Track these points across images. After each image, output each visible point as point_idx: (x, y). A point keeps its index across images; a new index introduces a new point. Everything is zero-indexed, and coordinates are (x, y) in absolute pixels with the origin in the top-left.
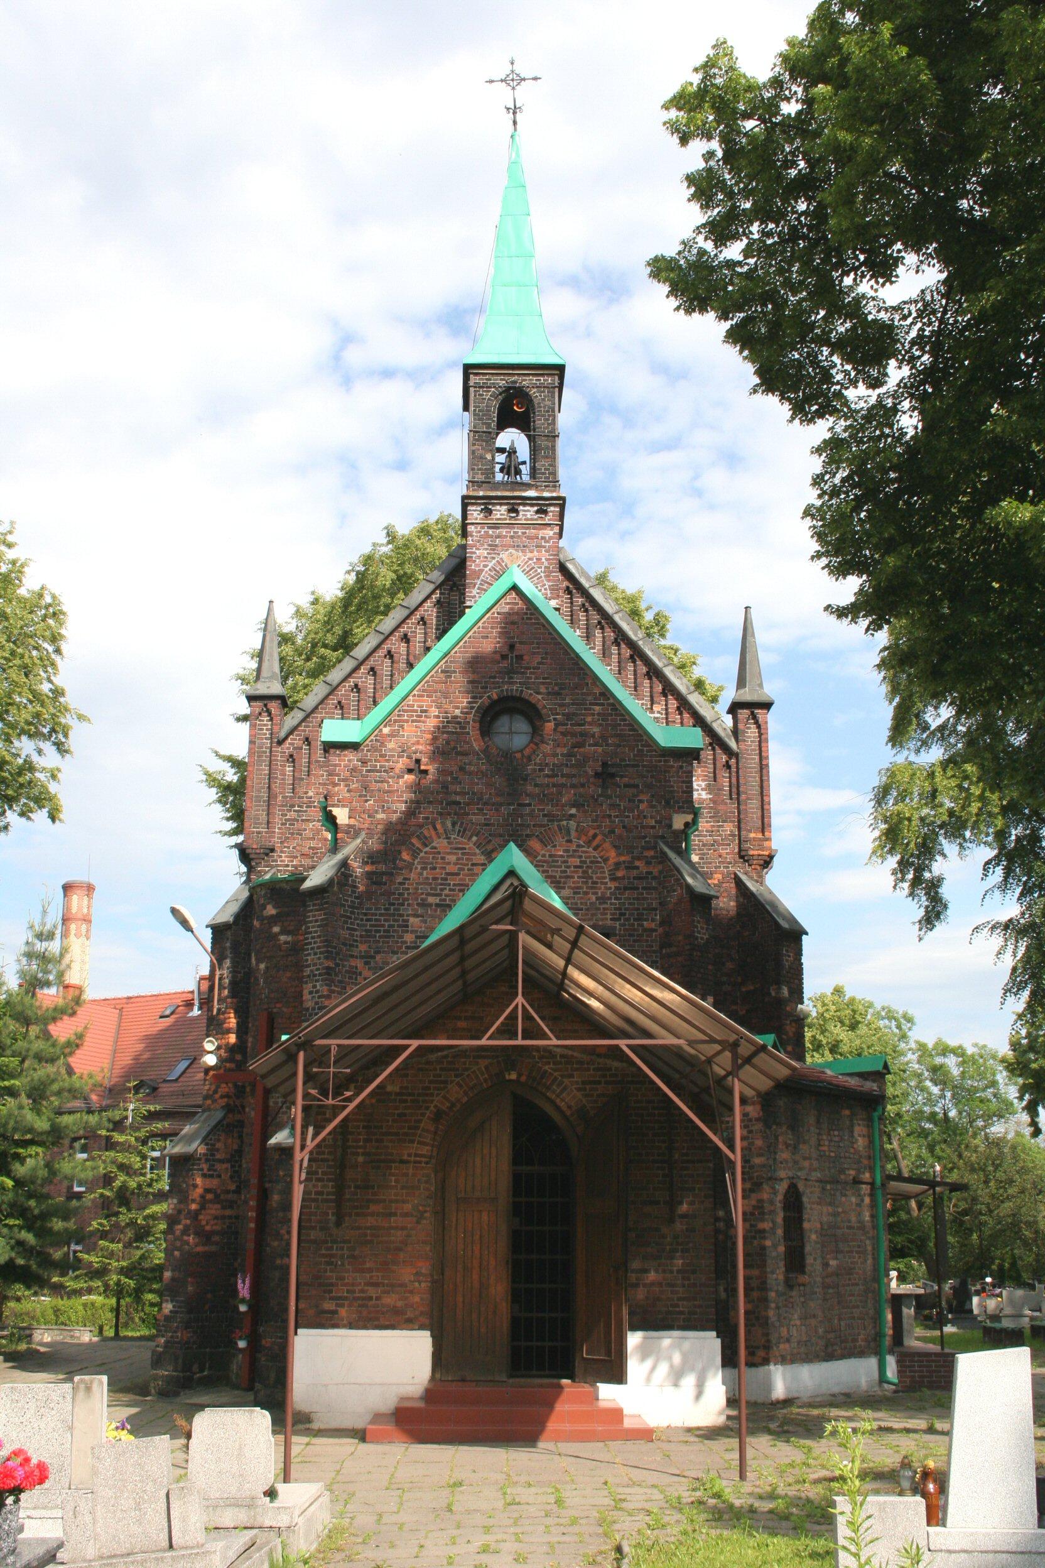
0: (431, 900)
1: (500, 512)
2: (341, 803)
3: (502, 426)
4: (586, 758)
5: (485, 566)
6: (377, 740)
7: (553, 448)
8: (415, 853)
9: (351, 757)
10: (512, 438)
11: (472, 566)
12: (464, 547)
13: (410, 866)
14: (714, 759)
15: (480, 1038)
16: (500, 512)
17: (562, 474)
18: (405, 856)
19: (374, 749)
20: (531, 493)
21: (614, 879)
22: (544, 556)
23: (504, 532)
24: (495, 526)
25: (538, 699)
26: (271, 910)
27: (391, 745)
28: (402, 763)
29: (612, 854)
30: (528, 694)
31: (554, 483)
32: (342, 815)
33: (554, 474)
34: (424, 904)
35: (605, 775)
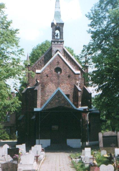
0: (49, 91)
1: (56, 43)
2: (38, 80)
3: (56, 30)
4: (67, 75)
5: (63, 78)
6: (42, 73)
7: (63, 34)
8: (47, 86)
9: (40, 75)
10: (57, 32)
11: (53, 49)
12: (51, 46)
13: (46, 87)
14: (59, 44)
15: (51, 57)
16: (56, 43)
17: (64, 38)
18: (46, 86)
19: (42, 73)
20: (60, 40)
21: (70, 88)
22: (62, 48)
23: (56, 45)
24: (55, 44)
25: (61, 68)
26: (30, 91)
27: (44, 73)
28: (45, 75)
29: (70, 86)
30: (62, 71)
31: (63, 39)
32: (38, 81)
33: (63, 38)
34: (48, 92)
35: (69, 77)
